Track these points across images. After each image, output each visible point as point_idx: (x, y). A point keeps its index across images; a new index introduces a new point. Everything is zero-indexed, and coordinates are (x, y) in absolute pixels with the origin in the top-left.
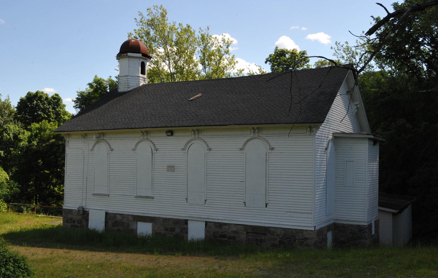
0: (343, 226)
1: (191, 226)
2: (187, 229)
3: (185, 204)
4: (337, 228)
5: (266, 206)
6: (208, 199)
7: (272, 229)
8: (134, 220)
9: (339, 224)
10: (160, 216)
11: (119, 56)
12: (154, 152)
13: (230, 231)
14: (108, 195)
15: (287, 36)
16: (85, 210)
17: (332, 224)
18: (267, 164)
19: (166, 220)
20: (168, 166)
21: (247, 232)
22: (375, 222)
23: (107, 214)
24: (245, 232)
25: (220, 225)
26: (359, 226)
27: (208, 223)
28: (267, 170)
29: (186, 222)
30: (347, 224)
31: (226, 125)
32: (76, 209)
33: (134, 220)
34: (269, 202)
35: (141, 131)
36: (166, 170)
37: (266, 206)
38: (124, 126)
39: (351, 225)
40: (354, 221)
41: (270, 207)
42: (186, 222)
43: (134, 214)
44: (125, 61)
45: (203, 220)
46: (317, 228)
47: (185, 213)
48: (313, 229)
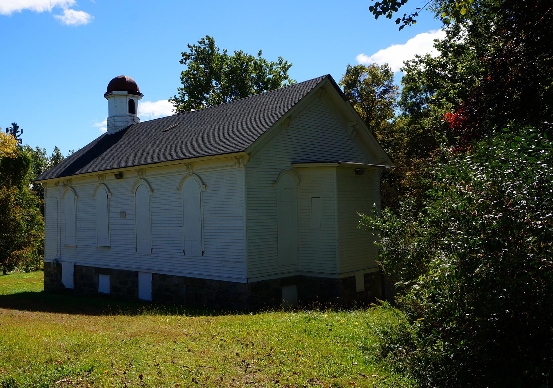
2: (137, 282)
3: (200, 258)
6: (153, 247)
10: (116, 268)
11: (106, 96)
14: (110, 247)
16: (59, 262)
19: (120, 272)
20: (121, 212)
23: (75, 266)
25: (164, 277)
26: (330, 279)
29: (136, 274)
31: (160, 162)
32: (51, 261)
35: (185, 163)
38: (240, 146)
40: (322, 273)
42: (136, 274)
44: (112, 99)
46: (250, 281)
48: (245, 282)
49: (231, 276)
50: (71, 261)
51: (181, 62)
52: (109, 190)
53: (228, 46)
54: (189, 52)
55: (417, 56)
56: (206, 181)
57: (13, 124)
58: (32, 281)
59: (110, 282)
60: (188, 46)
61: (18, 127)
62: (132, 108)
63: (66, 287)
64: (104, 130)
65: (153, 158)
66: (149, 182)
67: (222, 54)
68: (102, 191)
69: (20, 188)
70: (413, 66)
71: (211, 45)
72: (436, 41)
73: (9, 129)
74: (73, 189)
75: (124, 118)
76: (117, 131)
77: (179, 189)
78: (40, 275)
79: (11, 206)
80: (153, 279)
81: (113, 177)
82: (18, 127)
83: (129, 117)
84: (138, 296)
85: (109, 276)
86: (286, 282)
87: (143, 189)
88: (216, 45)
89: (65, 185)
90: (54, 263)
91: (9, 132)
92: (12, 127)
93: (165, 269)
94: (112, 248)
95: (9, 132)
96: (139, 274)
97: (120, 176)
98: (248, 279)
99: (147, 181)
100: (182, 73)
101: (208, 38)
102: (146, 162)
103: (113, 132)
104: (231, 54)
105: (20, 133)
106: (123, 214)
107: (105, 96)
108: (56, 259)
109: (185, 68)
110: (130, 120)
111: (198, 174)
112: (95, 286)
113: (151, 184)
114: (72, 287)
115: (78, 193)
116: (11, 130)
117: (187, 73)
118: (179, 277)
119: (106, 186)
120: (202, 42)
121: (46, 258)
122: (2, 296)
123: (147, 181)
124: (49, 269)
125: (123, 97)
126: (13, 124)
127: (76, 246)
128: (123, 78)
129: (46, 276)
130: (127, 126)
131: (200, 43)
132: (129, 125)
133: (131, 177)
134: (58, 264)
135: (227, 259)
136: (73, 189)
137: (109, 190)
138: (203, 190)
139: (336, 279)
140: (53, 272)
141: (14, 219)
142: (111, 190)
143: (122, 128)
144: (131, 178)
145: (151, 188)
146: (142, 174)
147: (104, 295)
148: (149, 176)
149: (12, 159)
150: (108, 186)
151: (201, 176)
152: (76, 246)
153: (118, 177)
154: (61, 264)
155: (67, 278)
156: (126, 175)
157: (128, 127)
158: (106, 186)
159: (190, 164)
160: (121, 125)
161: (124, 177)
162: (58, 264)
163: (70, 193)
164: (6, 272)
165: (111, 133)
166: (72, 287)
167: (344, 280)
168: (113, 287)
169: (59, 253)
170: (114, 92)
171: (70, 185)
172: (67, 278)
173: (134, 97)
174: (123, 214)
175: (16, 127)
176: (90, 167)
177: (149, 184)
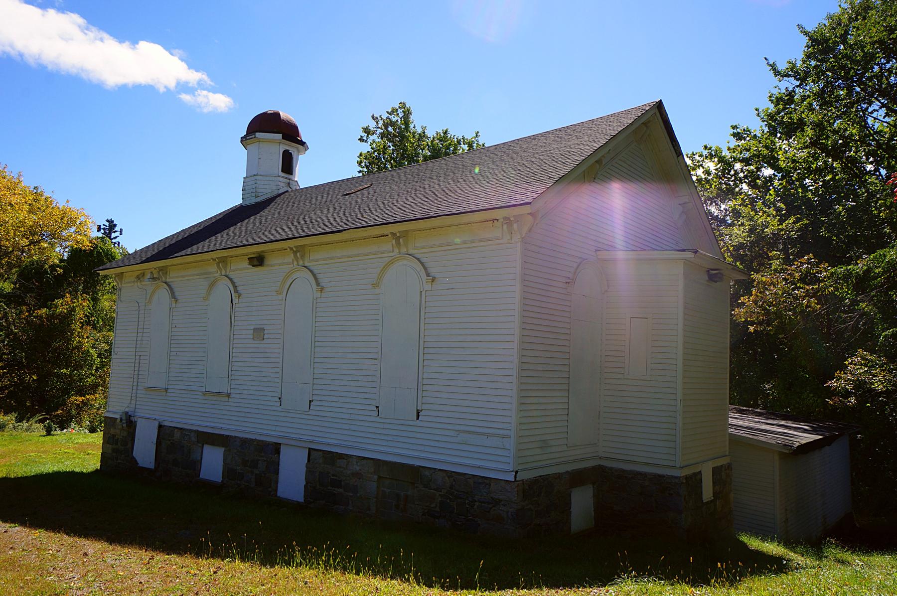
0: (623, 475)
1: (286, 456)
4: (606, 479)
5: (418, 418)
6: (315, 398)
7: (427, 473)
8: (198, 442)
9: (611, 469)
11: (243, 140)
12: (235, 300)
13: (349, 472)
14: (229, 395)
15: (154, 41)
17: (594, 468)
18: (422, 317)
20: (254, 329)
21: (380, 477)
22: (716, 471)
23: (160, 427)
24: (376, 477)
25: (332, 457)
26: (661, 476)
27: (312, 453)
28: (422, 329)
30: (631, 472)
32: (118, 416)
33: (198, 442)
34: (425, 407)
35: (392, 234)
36: (251, 337)
37: (418, 418)
39: (640, 473)
41: (236, 400)
43: (200, 429)
44: (253, 147)
45: (304, 445)
47: (278, 428)
49: (479, 463)
50: (154, 417)
51: (361, 140)
52: (235, 287)
53: (428, 122)
54: (372, 125)
55: (706, 147)
56: (432, 270)
57: (108, 221)
58: (77, 450)
59: (225, 460)
60: (373, 117)
61: (115, 225)
62: (288, 165)
63: (141, 465)
64: (241, 201)
65: (326, 226)
66: (315, 272)
67: (419, 130)
68: (223, 288)
69: (95, 300)
70: (698, 162)
71: (407, 114)
72: (734, 127)
73: (102, 227)
74: (169, 286)
75: (273, 179)
76: (259, 200)
77: (375, 285)
78: (97, 438)
79: (76, 326)
80: (309, 460)
81: (246, 264)
82: (115, 225)
83: (281, 179)
84: (276, 490)
85: (223, 449)
86: (578, 478)
87: (303, 284)
88: (412, 118)
89: (154, 279)
90: (121, 420)
91: (102, 231)
92: (107, 224)
93: (334, 439)
94: (232, 395)
95: (102, 231)
96: (283, 450)
97: (258, 261)
98: (516, 472)
99: (311, 271)
100: (361, 155)
101: (403, 105)
102: (312, 232)
103: (253, 201)
104: (430, 133)
105: (118, 234)
106: (259, 333)
107: (242, 141)
108: (127, 413)
109: (366, 148)
110: (283, 184)
111: (418, 256)
112: (196, 465)
113: (318, 276)
114: (152, 466)
115: (177, 294)
116: (104, 229)
117: (368, 157)
118: (364, 458)
119: (231, 279)
120: (394, 111)
121: (110, 409)
122: (5, 480)
123: (311, 271)
124: (112, 431)
125: (274, 145)
126: (108, 221)
127: (166, 390)
128: (277, 115)
129: (107, 440)
130: (276, 193)
131: (390, 114)
132: (281, 191)
133: (280, 264)
134: (129, 422)
135: (472, 429)
136: (169, 286)
137: (235, 287)
138: (428, 287)
139: (676, 477)
140: (119, 435)
141: (79, 348)
142: (239, 288)
143: (268, 196)
144: (279, 265)
145: (318, 284)
146: (303, 257)
147: (209, 485)
148: (317, 260)
149: (85, 251)
150: (235, 280)
151: (423, 260)
152: (166, 390)
153: (256, 263)
154: (136, 422)
155: (144, 450)
156: (270, 260)
157: (279, 195)
158: (231, 279)
159: (405, 234)
160: (266, 190)
161: (267, 262)
162: (129, 422)
163: (163, 293)
164: (51, 430)
165: (248, 202)
166: (152, 466)
167: (687, 478)
168: (228, 471)
169: (133, 402)
170: (258, 134)
171: (164, 279)
172: (144, 450)
173: (292, 148)
174: (259, 333)
175: (112, 225)
176: (203, 246)
177: (314, 275)
